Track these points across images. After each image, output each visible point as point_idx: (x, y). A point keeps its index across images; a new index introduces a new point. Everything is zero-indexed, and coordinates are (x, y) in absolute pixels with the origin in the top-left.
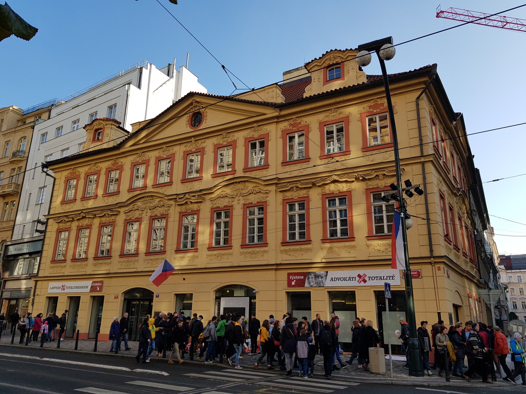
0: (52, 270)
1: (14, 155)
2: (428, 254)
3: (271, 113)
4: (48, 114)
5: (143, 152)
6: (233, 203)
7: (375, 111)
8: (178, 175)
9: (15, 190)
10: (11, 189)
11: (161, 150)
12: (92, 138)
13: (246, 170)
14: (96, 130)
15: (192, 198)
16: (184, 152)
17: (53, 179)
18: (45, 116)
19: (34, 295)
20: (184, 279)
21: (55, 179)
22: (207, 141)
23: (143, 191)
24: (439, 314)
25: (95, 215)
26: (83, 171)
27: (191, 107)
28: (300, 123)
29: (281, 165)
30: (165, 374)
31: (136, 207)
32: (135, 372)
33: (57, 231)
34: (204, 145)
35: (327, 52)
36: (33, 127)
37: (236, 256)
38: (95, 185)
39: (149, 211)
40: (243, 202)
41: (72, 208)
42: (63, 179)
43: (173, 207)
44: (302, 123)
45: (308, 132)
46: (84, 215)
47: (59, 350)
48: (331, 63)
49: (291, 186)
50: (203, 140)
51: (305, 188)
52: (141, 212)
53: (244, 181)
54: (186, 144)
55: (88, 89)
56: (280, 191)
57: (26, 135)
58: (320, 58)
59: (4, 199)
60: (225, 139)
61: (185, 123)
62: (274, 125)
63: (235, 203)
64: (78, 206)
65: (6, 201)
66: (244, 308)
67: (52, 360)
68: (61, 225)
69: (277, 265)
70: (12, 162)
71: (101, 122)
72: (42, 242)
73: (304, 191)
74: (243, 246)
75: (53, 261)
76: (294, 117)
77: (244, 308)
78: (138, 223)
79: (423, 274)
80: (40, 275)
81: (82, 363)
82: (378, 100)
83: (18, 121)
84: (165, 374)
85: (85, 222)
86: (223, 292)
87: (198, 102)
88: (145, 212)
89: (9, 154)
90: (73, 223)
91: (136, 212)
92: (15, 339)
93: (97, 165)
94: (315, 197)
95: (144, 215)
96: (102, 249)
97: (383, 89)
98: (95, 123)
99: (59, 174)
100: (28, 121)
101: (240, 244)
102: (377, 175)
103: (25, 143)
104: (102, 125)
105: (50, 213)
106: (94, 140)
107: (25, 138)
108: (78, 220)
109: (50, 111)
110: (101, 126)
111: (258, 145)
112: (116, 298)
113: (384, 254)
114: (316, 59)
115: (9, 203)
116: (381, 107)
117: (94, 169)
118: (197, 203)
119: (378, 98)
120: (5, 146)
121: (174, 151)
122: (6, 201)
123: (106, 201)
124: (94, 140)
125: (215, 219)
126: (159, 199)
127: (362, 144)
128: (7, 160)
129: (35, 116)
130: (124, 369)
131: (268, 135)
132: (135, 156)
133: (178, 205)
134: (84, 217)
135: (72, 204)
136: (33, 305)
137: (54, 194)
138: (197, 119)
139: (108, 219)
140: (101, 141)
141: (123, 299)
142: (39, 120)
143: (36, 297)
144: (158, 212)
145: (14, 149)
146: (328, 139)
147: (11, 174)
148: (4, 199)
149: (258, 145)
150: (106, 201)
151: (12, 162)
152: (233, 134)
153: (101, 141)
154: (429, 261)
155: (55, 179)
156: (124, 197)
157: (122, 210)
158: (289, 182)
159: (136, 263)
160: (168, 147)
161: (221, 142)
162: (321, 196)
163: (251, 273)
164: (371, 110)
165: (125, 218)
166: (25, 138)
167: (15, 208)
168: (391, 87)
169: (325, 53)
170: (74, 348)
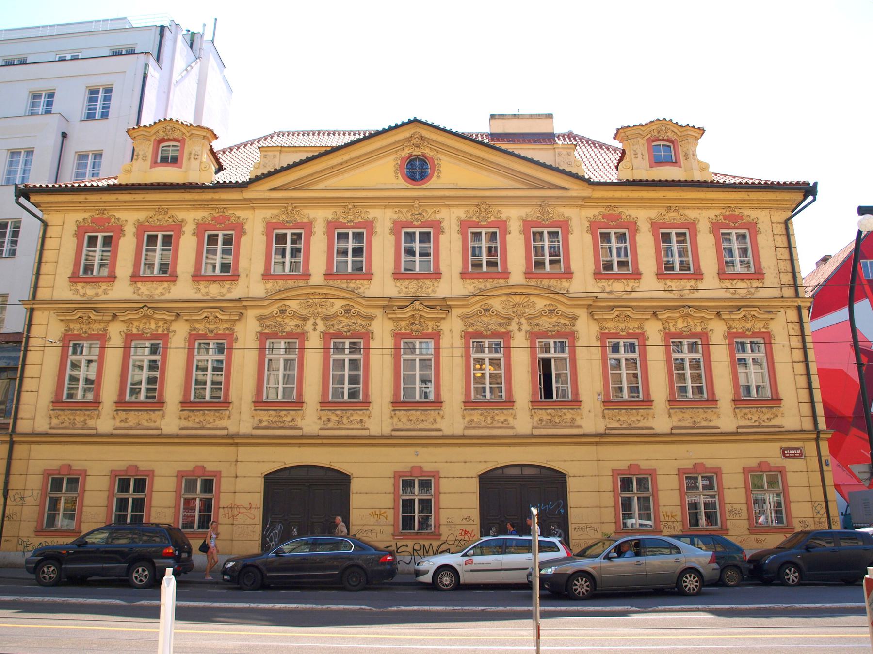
6: (510, 328)
21: (45, 225)
25: (178, 315)
29: (458, 276)
32: (136, 606)
39: (319, 322)
40: (528, 328)
53: (528, 294)
55: (158, 37)
61: (392, 169)
63: (309, 326)
67: (262, 605)
81: (202, 604)
87: (422, 138)
94: (180, 333)
111: (100, 241)
123: (204, 290)
127: (594, 268)
130: (118, 602)
137: (47, 255)
146: (208, 251)
149: (100, 241)
155: (45, 225)
163: (111, 447)
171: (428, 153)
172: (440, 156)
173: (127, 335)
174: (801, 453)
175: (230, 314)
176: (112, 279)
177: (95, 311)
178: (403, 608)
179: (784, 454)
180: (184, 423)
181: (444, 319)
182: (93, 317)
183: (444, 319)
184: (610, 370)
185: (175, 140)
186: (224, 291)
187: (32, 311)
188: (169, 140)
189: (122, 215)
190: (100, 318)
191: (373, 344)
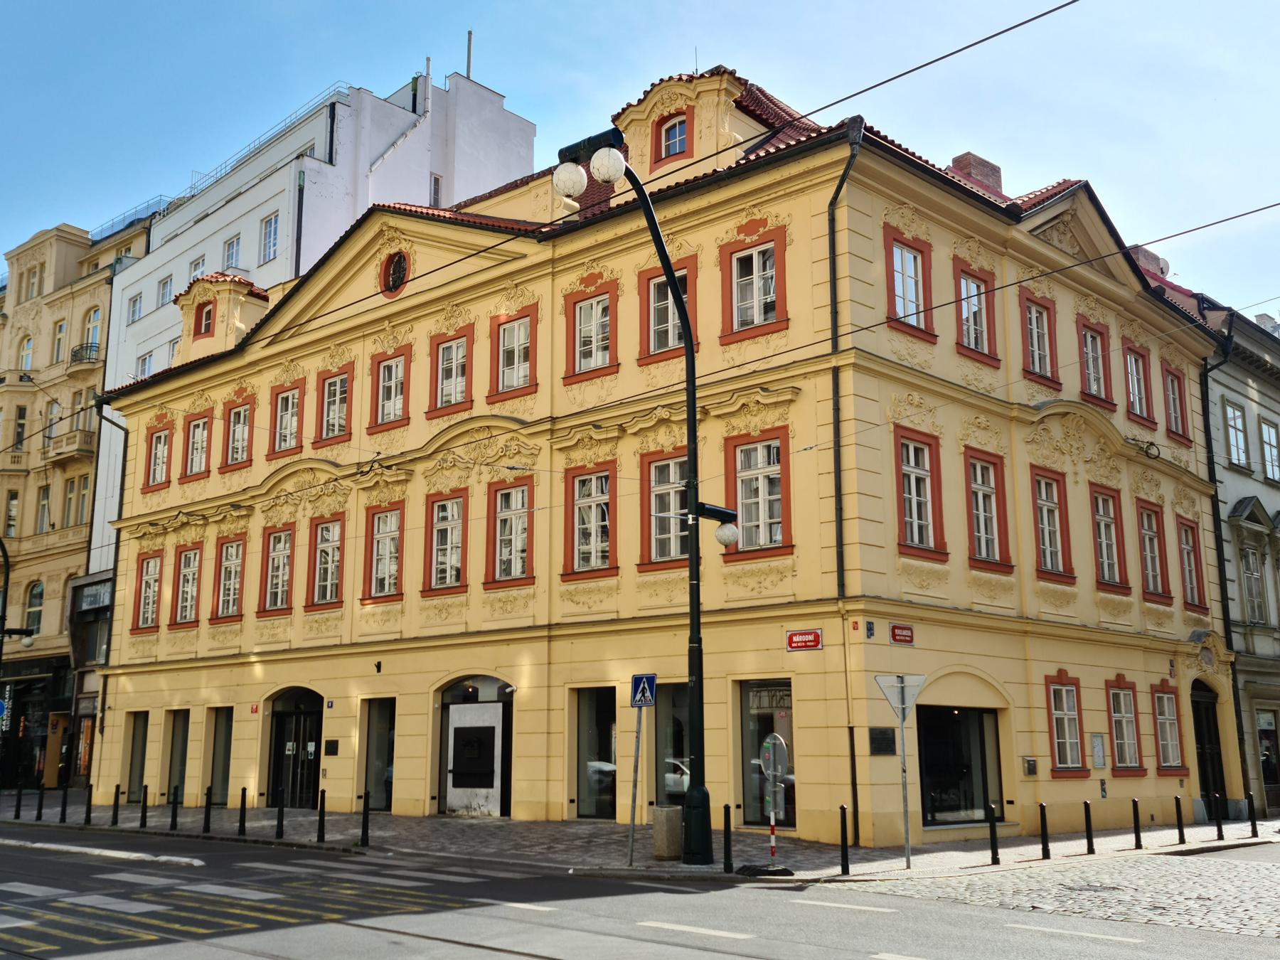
0: (133, 650)
1: (77, 356)
2: (833, 592)
3: (535, 252)
4: (144, 238)
5: (292, 361)
7: (748, 240)
8: (551, 360)
9: (85, 447)
10: (76, 446)
11: (441, 317)
12: (192, 327)
13: (494, 399)
14: (201, 307)
15: (386, 472)
16: (373, 357)
17: (123, 433)
18: (138, 246)
19: (103, 710)
20: (379, 666)
21: (127, 433)
22: (417, 325)
23: (465, 415)
24: (851, 729)
26: (180, 409)
27: (381, 241)
28: (600, 275)
30: (197, 863)
31: (450, 458)
33: (566, 477)
34: (410, 337)
35: (662, 80)
36: (110, 281)
37: (477, 609)
38: (295, 418)
41: (164, 502)
42: (143, 432)
43: (354, 492)
44: (605, 275)
45: (782, 246)
46: (185, 520)
47: (175, 832)
48: (666, 114)
49: (578, 436)
50: (408, 326)
51: (776, 404)
52: (464, 474)
54: (375, 337)
56: (560, 449)
57: (97, 302)
58: (640, 102)
59: (64, 470)
60: (453, 321)
62: (548, 280)
63: (472, 481)
64: (176, 496)
65: (69, 475)
66: (493, 728)
68: (145, 543)
69: (550, 627)
70: (72, 376)
71: (208, 285)
72: (109, 584)
73: (606, 448)
74: (646, 565)
75: (135, 630)
76: (586, 260)
77: (493, 728)
78: (158, 560)
79: (826, 639)
80: (113, 662)
82: (755, 210)
83: (81, 263)
84: (197, 863)
85: (190, 535)
86: (458, 691)
88: (300, 508)
89: (66, 355)
90: (621, 444)
91: (284, 508)
92: (69, 810)
93: (207, 394)
95: (299, 515)
96: (380, 576)
97: (643, 223)
98: (195, 290)
99: (134, 419)
100: (102, 264)
101: (483, 580)
102: (744, 405)
103: (96, 323)
104: (210, 294)
105: (125, 516)
106: (197, 333)
107: (95, 309)
108: (175, 530)
109: (148, 231)
110: (209, 297)
112: (255, 711)
113: (755, 594)
114: (629, 105)
115: (76, 480)
116: (761, 230)
117: (201, 405)
118: (399, 482)
119: (754, 206)
120: (55, 334)
121: (472, 317)
122: (69, 475)
124: (197, 333)
125: (653, 484)
126: (509, 436)
128: (59, 371)
129: (118, 247)
131: (694, 258)
132: (277, 371)
133: (364, 489)
134: (184, 525)
135: (396, 433)
136: (102, 731)
138: (395, 274)
139: (232, 527)
140: (686, 152)
141: (268, 712)
142: (124, 260)
143: (108, 713)
144: (325, 508)
145: (75, 343)
147: (73, 404)
148: (64, 470)
150: (228, 484)
151: (72, 376)
152: (467, 307)
153: (686, 152)
154: (834, 608)
155: (127, 433)
156: (419, 433)
157: (420, 468)
158: (572, 427)
159: (531, 604)
160: (339, 345)
161: (444, 330)
162: (638, 457)
163: (182, 674)
164: (742, 237)
165: (425, 492)
166: (95, 309)
167: (88, 493)
168: (658, 217)
169: (649, 89)
170: (58, 820)
171: (404, 246)
172: (416, 247)
173: (642, 456)
174: (912, 637)
175: (608, 429)
176: (784, 324)
177: (764, 390)
178: (29, 844)
179: (894, 636)
180: (216, 644)
181: (791, 401)
182: (595, 437)
183: (791, 401)
184: (572, 532)
185: (679, 113)
186: (603, 393)
187: (119, 531)
188: (671, 116)
189: (254, 381)
190: (604, 436)
191: (794, 445)
